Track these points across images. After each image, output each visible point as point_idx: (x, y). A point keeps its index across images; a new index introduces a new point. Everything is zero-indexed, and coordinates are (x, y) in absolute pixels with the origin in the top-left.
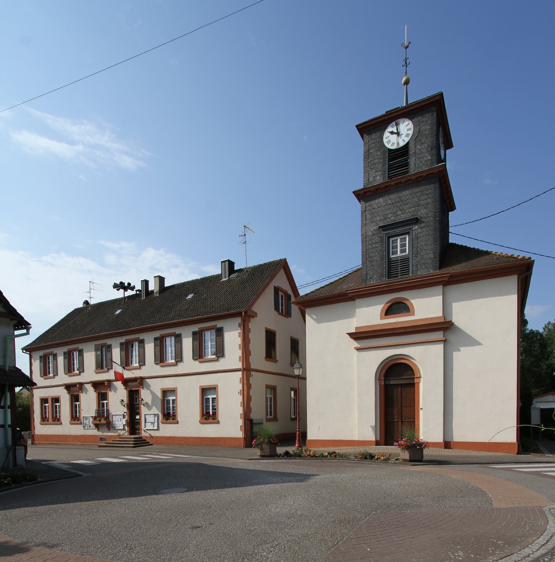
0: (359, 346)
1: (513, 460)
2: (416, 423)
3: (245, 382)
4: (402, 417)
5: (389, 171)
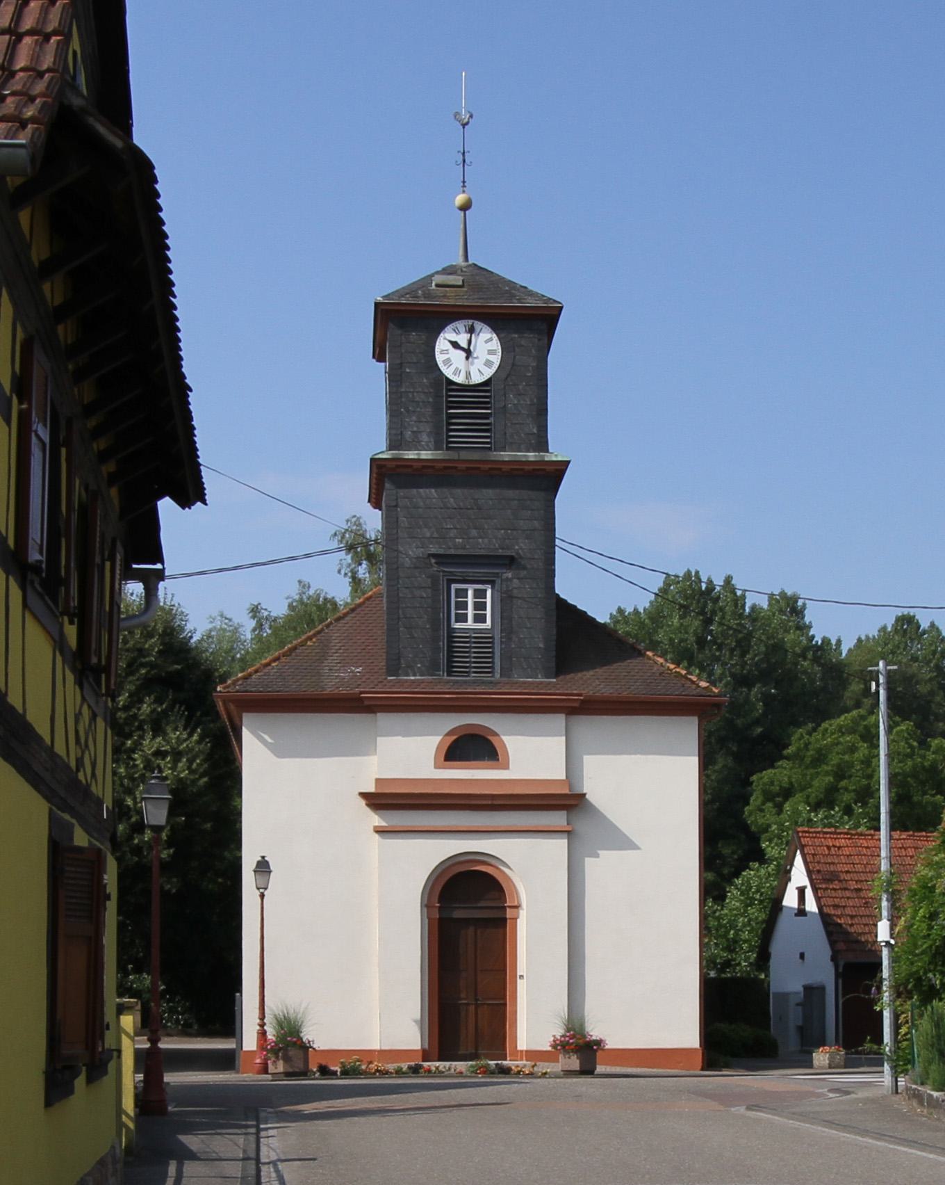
0: (384, 824)
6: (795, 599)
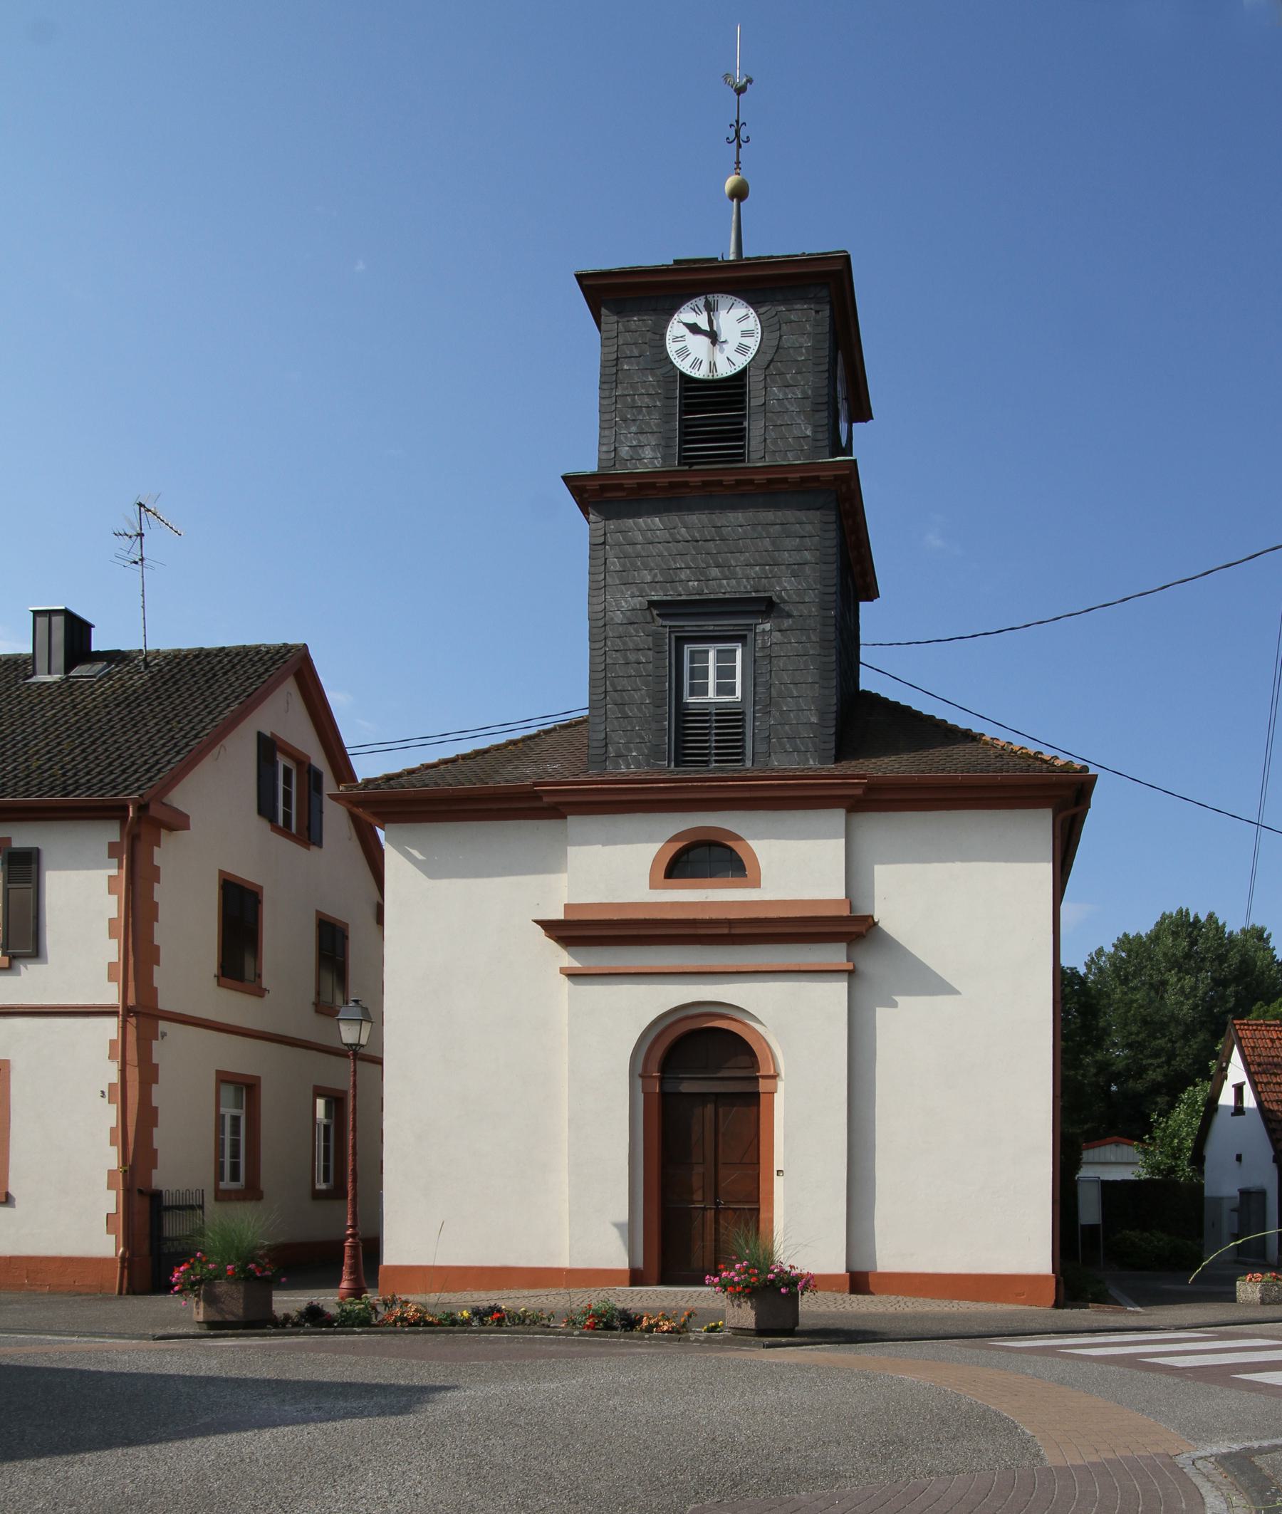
1: (1050, 1325)
2: (762, 1215)
3: (132, 1055)
4: (716, 1196)
5: (682, 442)
6: (1262, 930)
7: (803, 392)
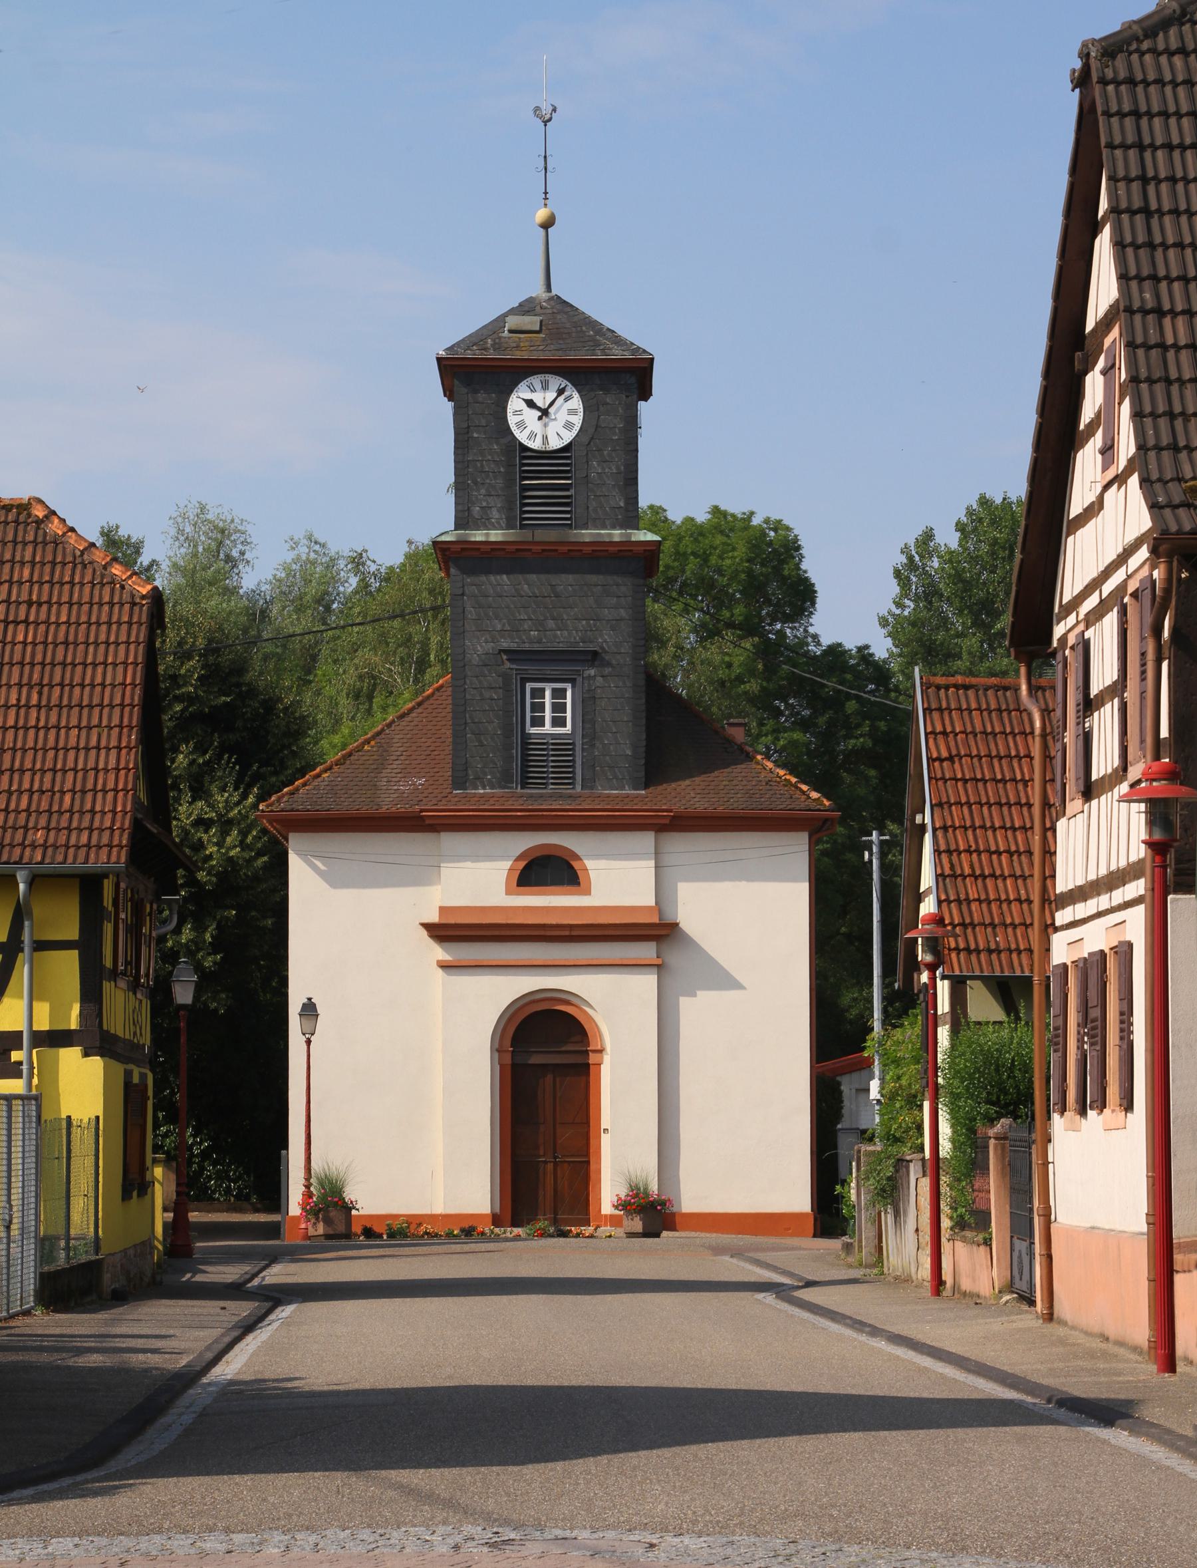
2: (593, 1167)
4: (555, 1152)
7: (618, 468)
